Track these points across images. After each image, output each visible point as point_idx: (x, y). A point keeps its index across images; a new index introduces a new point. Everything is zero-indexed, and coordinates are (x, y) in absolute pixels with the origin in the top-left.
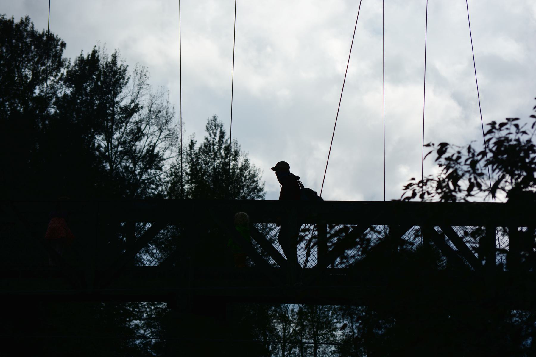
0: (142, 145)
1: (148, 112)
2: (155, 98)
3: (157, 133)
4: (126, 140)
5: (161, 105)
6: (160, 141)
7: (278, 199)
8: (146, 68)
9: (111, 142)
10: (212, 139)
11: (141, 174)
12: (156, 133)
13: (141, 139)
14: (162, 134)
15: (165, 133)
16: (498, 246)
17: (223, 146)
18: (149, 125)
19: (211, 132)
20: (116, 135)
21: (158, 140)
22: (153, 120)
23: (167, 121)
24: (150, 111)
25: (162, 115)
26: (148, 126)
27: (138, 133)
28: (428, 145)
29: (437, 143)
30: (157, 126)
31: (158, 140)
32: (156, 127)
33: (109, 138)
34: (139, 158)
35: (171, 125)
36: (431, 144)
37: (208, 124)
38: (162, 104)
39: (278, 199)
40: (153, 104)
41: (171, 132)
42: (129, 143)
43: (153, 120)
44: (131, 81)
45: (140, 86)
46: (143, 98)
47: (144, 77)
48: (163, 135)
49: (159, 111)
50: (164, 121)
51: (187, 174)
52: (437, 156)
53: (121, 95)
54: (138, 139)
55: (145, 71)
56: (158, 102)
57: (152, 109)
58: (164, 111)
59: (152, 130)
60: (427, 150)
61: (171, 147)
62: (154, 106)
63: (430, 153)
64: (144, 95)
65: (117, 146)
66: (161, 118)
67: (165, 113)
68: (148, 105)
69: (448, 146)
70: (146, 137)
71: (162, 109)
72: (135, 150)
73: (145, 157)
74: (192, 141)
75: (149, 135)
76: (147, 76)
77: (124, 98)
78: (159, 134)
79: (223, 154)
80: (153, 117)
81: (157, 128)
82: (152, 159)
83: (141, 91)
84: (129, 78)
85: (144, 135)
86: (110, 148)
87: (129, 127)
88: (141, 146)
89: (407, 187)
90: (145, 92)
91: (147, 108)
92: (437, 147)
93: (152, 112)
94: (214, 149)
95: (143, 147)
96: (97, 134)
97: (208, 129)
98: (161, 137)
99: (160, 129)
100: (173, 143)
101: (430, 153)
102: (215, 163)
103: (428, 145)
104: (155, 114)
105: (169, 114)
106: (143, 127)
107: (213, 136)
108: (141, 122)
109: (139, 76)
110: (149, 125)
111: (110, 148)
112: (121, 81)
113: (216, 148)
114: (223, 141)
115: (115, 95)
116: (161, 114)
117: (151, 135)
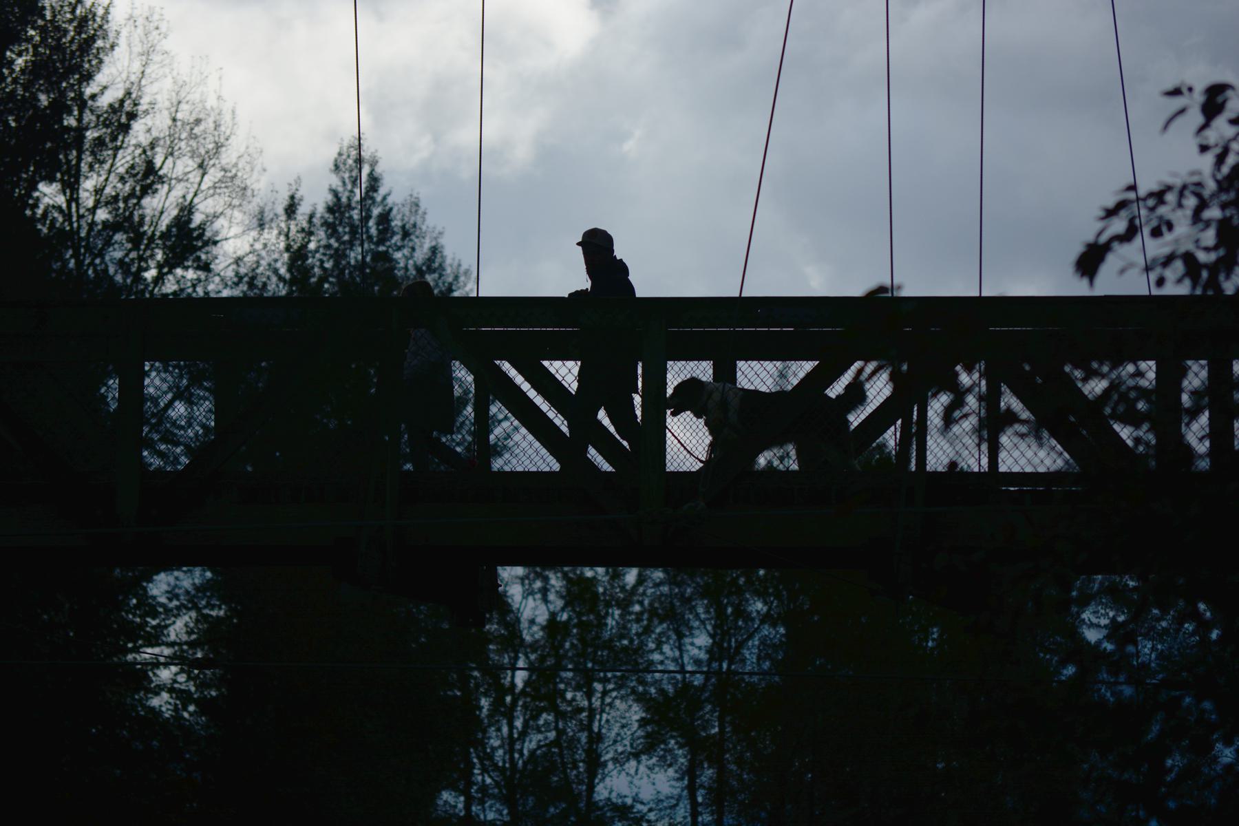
0: (160, 207)
1: (170, 122)
2: (187, 88)
3: (195, 177)
4: (118, 195)
5: (200, 105)
6: (201, 196)
7: (640, 293)
8: (157, 9)
9: (77, 200)
10: (347, 194)
11: (159, 279)
12: (190, 176)
13: (156, 191)
14: (206, 178)
15: (213, 175)
16: (528, 638)
17: (376, 211)
18: (172, 154)
19: (347, 175)
20: (88, 184)
21: (196, 195)
22: (183, 144)
23: (218, 146)
24: (174, 120)
25: (205, 132)
26: (170, 159)
27: (146, 176)
28: (1176, 92)
29: (1200, 87)
30: (192, 157)
31: (196, 195)
32: (190, 162)
33: (71, 186)
34: (152, 239)
35: (228, 157)
36: (1185, 90)
37: (340, 154)
38: (203, 101)
39: (640, 293)
40: (179, 102)
41: (229, 174)
42: (126, 200)
43: (183, 144)
44: (122, 41)
45: (147, 54)
46: (155, 87)
47: (155, 33)
48: (208, 181)
49: (198, 122)
50: (211, 146)
51: (281, 278)
52: (1200, 119)
53: (101, 78)
54: (147, 190)
55: (156, 17)
56: (195, 97)
57: (179, 116)
58: (211, 120)
59: (180, 169)
60: (1178, 102)
61: (229, 212)
62: (183, 106)
63: (1182, 111)
64: (157, 80)
65: (93, 211)
66: (202, 139)
67: (212, 126)
68: (167, 104)
69: (1229, 93)
70: (166, 187)
71: (202, 116)
72: (142, 217)
73: (164, 236)
74: (292, 197)
75: (173, 182)
76: (163, 29)
77: (110, 80)
78: (198, 179)
79: (373, 231)
80: (184, 136)
81: (192, 164)
82: (187, 240)
83: (148, 71)
84: (118, 33)
85: (161, 180)
86: (75, 215)
87: (123, 161)
88: (154, 210)
89: (1110, 213)
90: (161, 73)
91: (166, 113)
92: (1199, 98)
93: (179, 123)
94: (351, 217)
95: (157, 214)
96: (43, 179)
97: (337, 167)
98: (203, 187)
99: (201, 166)
100: (236, 202)
101: (1182, 111)
102: (352, 255)
103: (1176, 92)
104: (188, 128)
105: (223, 128)
106: (158, 161)
107: (349, 187)
108: (152, 148)
109: (140, 30)
110: (172, 154)
111: (75, 215)
112: (99, 43)
113: (355, 214)
114: (373, 199)
115: (88, 77)
116: (201, 127)
117: (179, 180)
